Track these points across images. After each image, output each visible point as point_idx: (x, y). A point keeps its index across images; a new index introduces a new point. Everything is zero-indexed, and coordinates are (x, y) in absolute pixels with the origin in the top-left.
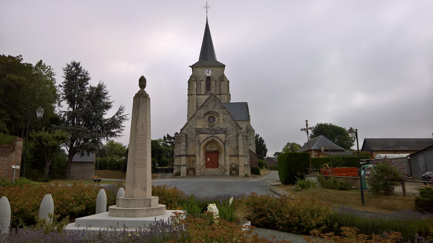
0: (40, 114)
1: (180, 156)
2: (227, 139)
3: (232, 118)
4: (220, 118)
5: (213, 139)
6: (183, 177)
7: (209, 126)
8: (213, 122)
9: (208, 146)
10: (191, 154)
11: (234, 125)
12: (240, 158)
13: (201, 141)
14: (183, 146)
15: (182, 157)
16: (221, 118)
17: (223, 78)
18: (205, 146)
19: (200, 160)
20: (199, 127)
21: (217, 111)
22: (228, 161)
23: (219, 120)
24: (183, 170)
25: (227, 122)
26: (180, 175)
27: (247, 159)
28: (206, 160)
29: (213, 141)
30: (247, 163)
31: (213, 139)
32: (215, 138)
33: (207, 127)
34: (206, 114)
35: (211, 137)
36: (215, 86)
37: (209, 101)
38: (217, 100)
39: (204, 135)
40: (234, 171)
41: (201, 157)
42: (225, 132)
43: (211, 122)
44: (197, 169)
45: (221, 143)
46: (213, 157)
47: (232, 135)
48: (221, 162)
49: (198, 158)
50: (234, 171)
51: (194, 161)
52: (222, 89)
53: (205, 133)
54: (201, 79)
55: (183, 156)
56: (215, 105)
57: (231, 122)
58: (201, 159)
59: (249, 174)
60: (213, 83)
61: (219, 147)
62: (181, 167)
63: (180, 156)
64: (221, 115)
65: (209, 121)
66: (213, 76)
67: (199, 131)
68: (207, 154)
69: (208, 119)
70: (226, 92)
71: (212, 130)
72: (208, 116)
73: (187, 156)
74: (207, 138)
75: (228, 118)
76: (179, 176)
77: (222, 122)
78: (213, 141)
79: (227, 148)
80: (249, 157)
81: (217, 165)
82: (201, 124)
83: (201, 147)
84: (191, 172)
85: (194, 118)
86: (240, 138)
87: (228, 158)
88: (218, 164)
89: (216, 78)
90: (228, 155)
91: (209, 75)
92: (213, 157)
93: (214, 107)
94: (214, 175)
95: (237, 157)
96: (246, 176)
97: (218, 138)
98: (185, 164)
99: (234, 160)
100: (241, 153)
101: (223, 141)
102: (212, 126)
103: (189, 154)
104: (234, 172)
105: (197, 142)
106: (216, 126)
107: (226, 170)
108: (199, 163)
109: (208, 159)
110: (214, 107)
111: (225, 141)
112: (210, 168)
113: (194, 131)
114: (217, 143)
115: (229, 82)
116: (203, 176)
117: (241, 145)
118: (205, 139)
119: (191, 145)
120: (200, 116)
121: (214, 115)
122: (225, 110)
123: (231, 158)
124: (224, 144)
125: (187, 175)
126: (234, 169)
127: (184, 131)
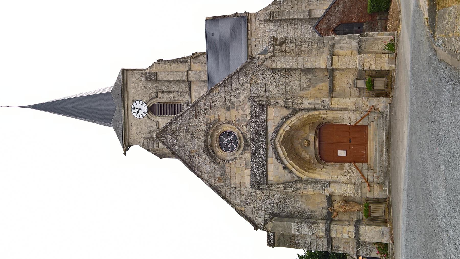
0: (306, 229)
1: (330, 240)
2: (281, 101)
3: (223, 83)
4: (222, 119)
5: (282, 143)
6: (392, 235)
7: (244, 150)
8: (235, 137)
9: (304, 154)
10: (325, 205)
11: (242, 78)
12: (338, 63)
13: (287, 177)
14: (299, 230)
15: (333, 235)
16: (223, 115)
17: (150, 75)
18: (304, 164)
19: (341, 180)
20: (248, 179)
21: (204, 127)
22: (346, 100)
23: (229, 122)
24: (370, 233)
25: (233, 100)
26: (386, 244)
27: (343, 44)
28: (342, 160)
29: (289, 142)
30: (354, 44)
31: (282, 143)
32: (279, 138)
33: (248, 155)
34: (214, 158)
35: (275, 148)
36: (171, 95)
37: (177, 146)
38: (175, 125)
39: (270, 168)
40: (378, 84)
41: (335, 178)
42: (263, 108)
43: (236, 143)
44: (370, 195)
45: (294, 119)
46: (335, 142)
47: (272, 87)
48: (349, 118)
49: (337, 190)
50: (378, 84)
51: (347, 200)
52: (178, 79)
53: (265, 165)
54: (155, 128)
55: (328, 231)
56: (187, 131)
57: (234, 87)
58: (340, 178)
59: (387, 37)
60: (164, 99)
61: (305, 123)
62: (362, 239)
63: (330, 240)
64: (215, 115)
65: (233, 149)
66: (147, 99)
67: (260, 181)
68: (325, 157)
69: (227, 150)
70: (184, 68)
71: (256, 143)
72: (220, 152)
73: (329, 219)
74: (278, 158)
75: (223, 94)
76: (390, 247)
77: (235, 117)
78: (289, 142)
79: (306, 103)
80: (337, 37)
81: (360, 131)
82: (241, 173)
83: (304, 177)
84: (378, 210)
85: (223, 190)
86: (278, 65)
87: (337, 103)
88: (356, 126)
89: (152, 91)
90: (327, 100)
91: (144, 108)
92: (335, 142)
93: (194, 134)
94: (389, 145)
95: (336, 73)
96: (392, 47)
97: (278, 128)
98: (352, 228)
99: (344, 82)
100: (321, 62)
101: (286, 112)
102: (245, 140)
103: (325, 211)
104: (380, 84)
105: (290, 190)
106: (244, 129)
107: (374, 109)
108: (351, 187)
109: (342, 153)
110: (194, 134)
111: (287, 108)
112: (366, 150)
113: (261, 194)
114: (294, 129)
115: (160, 61)
116: (389, 177)
117: (301, 62)
118: (280, 166)
119: (300, 205)
120: (218, 173)
121: (216, 135)
122: (202, 104)
123: (337, 89)
124: (296, 111)
125: (385, 222)
126: (371, 85)
127: (261, 220)
